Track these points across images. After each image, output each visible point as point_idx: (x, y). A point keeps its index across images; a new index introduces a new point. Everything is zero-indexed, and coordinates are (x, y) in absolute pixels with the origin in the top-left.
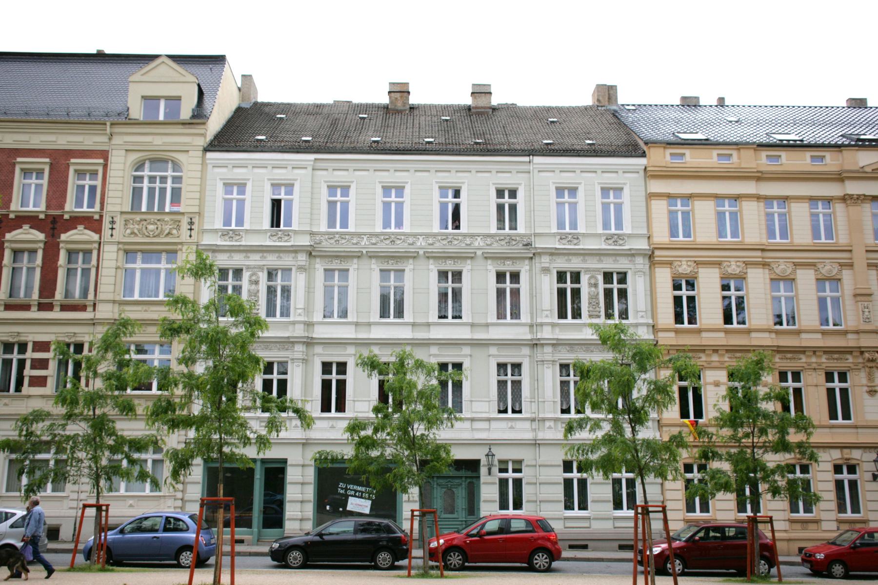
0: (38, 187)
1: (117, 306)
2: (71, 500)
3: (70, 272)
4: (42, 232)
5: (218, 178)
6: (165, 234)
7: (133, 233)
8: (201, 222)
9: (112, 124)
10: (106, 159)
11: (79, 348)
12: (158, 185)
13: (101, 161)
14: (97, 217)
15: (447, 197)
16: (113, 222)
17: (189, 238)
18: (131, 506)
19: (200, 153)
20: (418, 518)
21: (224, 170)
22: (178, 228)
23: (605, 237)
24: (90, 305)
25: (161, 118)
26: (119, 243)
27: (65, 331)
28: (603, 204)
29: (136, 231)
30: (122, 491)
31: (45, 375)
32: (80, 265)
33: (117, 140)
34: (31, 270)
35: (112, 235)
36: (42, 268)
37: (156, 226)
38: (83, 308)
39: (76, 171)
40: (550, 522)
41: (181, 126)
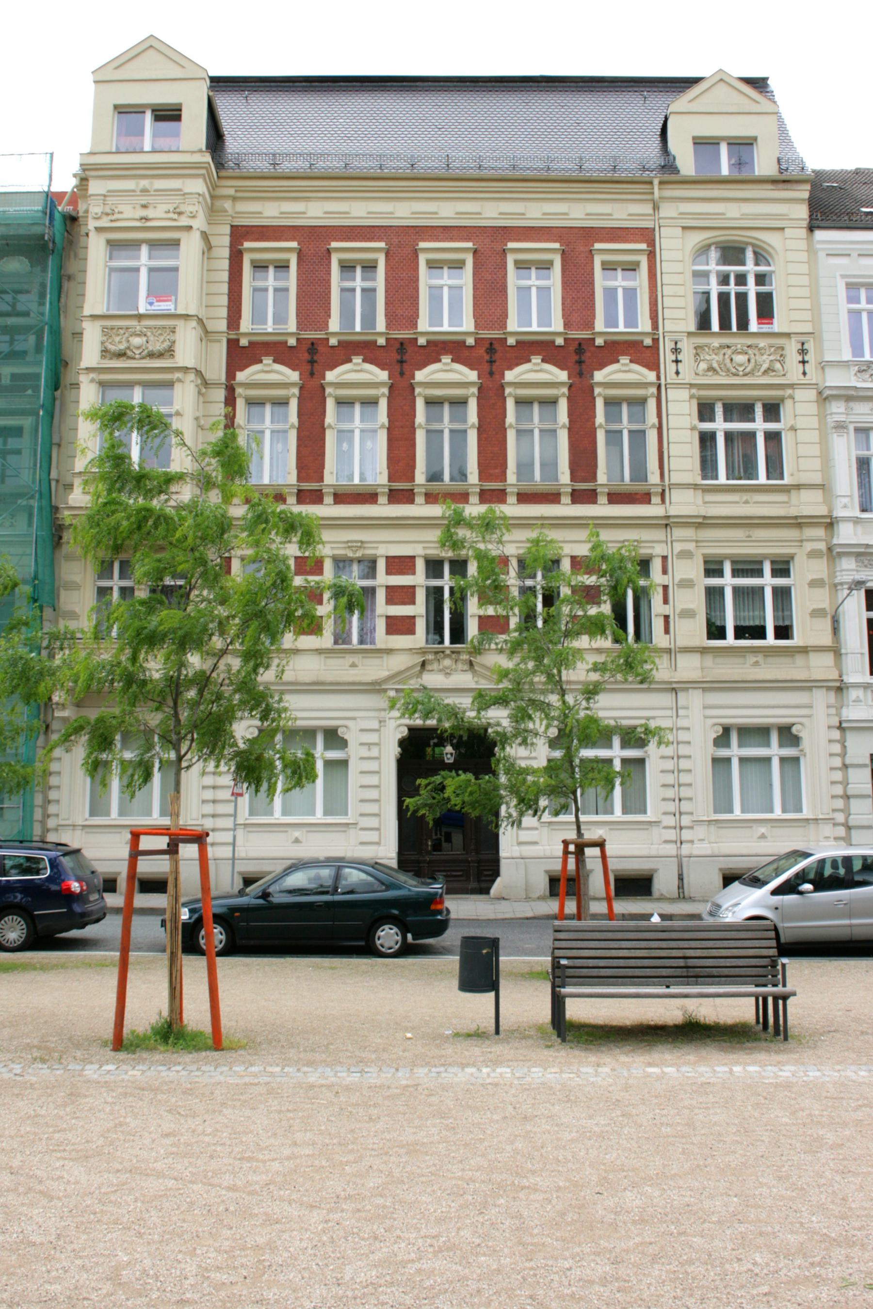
0: (281, 291)
1: (699, 492)
2: (665, 828)
3: (434, 435)
4: (562, 369)
5: (838, 274)
6: (762, 370)
7: (711, 369)
8: (820, 351)
9: (661, 183)
10: (652, 243)
11: (644, 565)
12: (732, 288)
13: (643, 246)
14: (648, 342)
15: (859, 302)
16: (676, 350)
17: (802, 377)
18: (763, 837)
19: (803, 233)
20: (573, 856)
21: (844, 261)
22: (782, 360)
23: (856, 368)
24: (656, 494)
25: (725, 171)
26: (692, 386)
27: (345, 539)
28: (850, 312)
29: (715, 365)
30: (277, 816)
31: (412, 614)
32: (625, 424)
33: (667, 210)
34: (459, 435)
35: (677, 373)
36: (479, 429)
37: (747, 357)
38: (645, 498)
39: (516, 262)
40: (93, 862)
41: (770, 186)
